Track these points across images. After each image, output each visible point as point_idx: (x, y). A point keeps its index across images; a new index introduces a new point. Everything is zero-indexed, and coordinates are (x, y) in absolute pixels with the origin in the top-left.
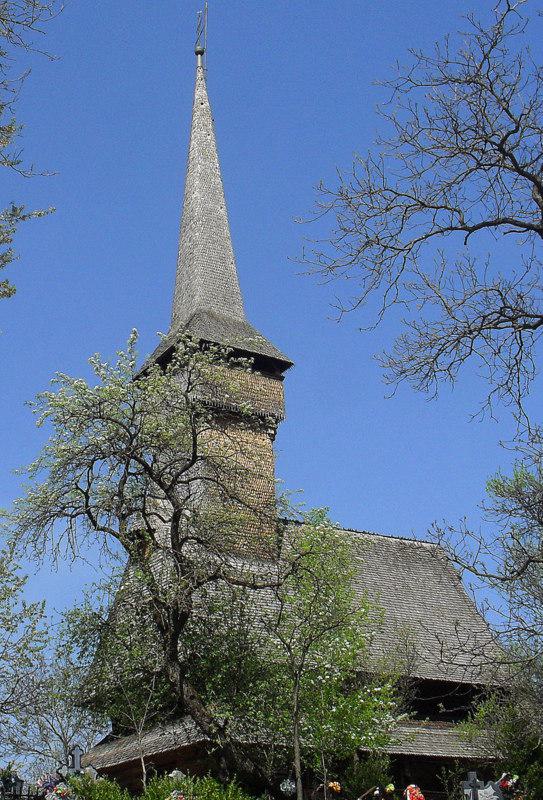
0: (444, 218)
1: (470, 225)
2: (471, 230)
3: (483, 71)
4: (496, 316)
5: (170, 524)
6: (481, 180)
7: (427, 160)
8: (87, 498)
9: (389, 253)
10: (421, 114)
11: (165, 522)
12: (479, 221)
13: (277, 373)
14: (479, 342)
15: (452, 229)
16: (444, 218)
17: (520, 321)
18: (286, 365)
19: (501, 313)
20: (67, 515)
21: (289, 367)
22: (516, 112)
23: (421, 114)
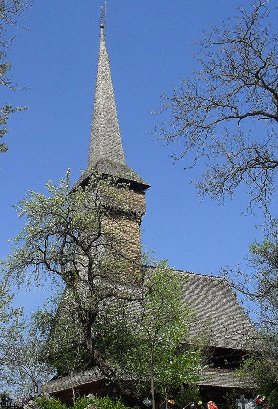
0: (227, 112)
1: (241, 115)
2: (241, 118)
3: (247, 36)
6: (246, 92)
11: (84, 267)
13: (142, 191)
15: (231, 117)
16: (227, 112)
17: (266, 164)
19: (257, 160)
21: (148, 188)
22: (264, 57)
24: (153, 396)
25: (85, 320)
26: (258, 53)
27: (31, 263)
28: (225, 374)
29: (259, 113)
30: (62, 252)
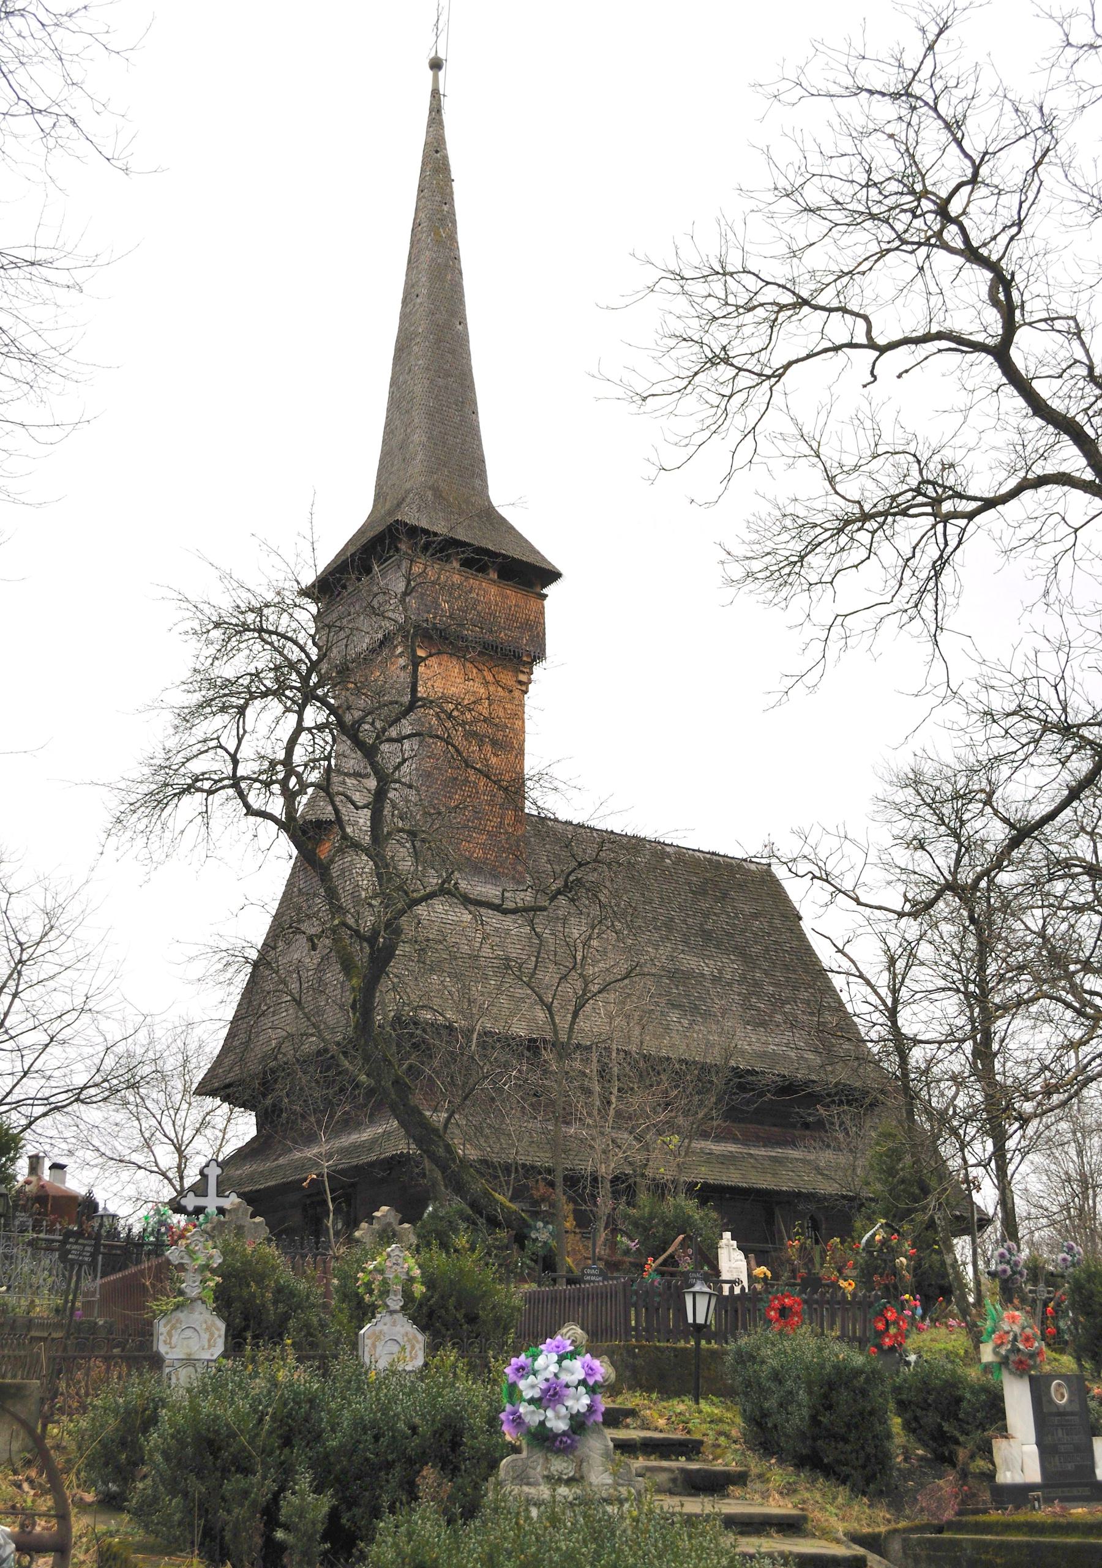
0: (840, 329)
1: (881, 341)
2: (882, 350)
3: (924, 74)
4: (909, 495)
5: (367, 812)
6: (900, 265)
7: (815, 226)
8: (235, 762)
9: (744, 380)
10: (810, 146)
11: (357, 808)
12: (898, 336)
13: (538, 590)
14: (145, 1042)
15: (851, 345)
16: (840, 329)
17: (947, 507)
18: (65, 1166)
19: (918, 491)
20: (202, 790)
21: (555, 580)
22: (974, 144)
23: (810, 146)
24: (964, 1519)
25: (1072, 378)
26: (954, 128)
27: (188, 789)
28: (762, 1152)
29: (940, 336)
30: (288, 761)
